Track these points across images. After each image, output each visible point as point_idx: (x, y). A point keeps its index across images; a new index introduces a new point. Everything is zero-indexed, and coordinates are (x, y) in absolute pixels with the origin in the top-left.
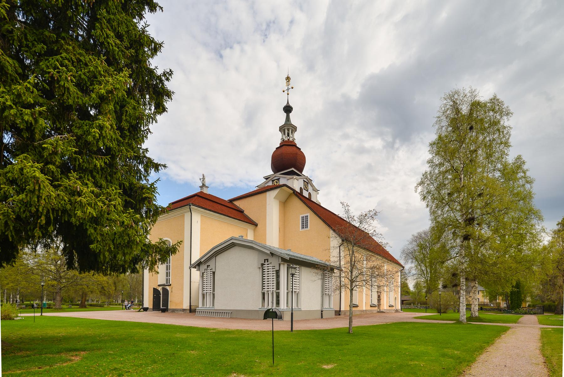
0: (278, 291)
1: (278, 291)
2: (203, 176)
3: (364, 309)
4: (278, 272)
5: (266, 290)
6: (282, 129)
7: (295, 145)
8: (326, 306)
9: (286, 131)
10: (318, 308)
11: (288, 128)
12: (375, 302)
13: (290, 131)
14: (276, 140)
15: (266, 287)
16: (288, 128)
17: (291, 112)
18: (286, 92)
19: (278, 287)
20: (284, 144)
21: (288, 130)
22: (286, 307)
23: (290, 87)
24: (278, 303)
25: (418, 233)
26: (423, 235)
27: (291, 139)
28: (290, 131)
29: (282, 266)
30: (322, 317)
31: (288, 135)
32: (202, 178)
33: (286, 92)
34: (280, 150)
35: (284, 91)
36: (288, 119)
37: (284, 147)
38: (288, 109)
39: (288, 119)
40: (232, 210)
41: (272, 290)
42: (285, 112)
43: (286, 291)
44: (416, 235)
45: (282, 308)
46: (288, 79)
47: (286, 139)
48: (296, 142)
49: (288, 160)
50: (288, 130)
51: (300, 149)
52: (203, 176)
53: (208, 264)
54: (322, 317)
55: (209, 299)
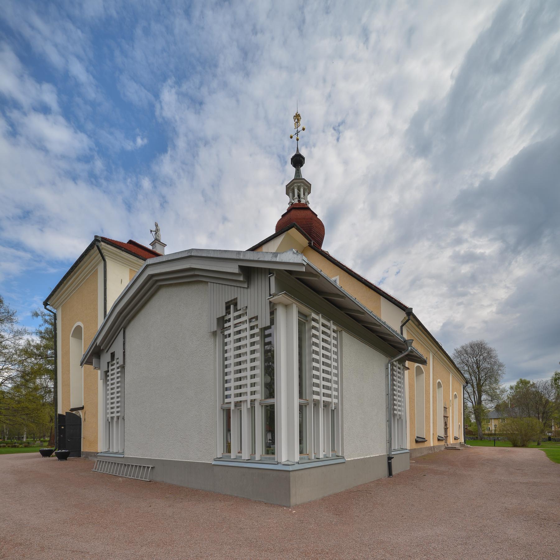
0: (270, 401)
1: (270, 401)
2: (157, 225)
3: (432, 445)
4: (266, 335)
5: (233, 400)
6: (290, 189)
7: (308, 209)
8: (395, 446)
9: (296, 191)
10: (380, 451)
11: (298, 187)
12: (442, 435)
13: (302, 190)
14: (283, 204)
15: (232, 392)
16: (298, 187)
17: (302, 166)
18: (295, 137)
19: (270, 389)
20: (293, 208)
21: (299, 190)
22: (297, 457)
23: (300, 128)
24: (270, 446)
25: (463, 347)
26: (469, 349)
27: (303, 201)
28: (302, 190)
29: (280, 313)
30: (390, 473)
31: (299, 196)
32: (154, 229)
33: (295, 137)
34: (287, 216)
35: (291, 137)
36: (298, 173)
37: (293, 212)
38: (298, 161)
39: (298, 173)
40: (329, 467)
41: (249, 398)
42: (294, 166)
43: (297, 401)
44: (460, 349)
45: (284, 459)
46: (297, 117)
47: (296, 201)
48: (311, 206)
49: (301, 222)
50: (299, 190)
51: (316, 215)
52: (157, 225)
53: (111, 351)
54: (390, 473)
55: (248, 428)
